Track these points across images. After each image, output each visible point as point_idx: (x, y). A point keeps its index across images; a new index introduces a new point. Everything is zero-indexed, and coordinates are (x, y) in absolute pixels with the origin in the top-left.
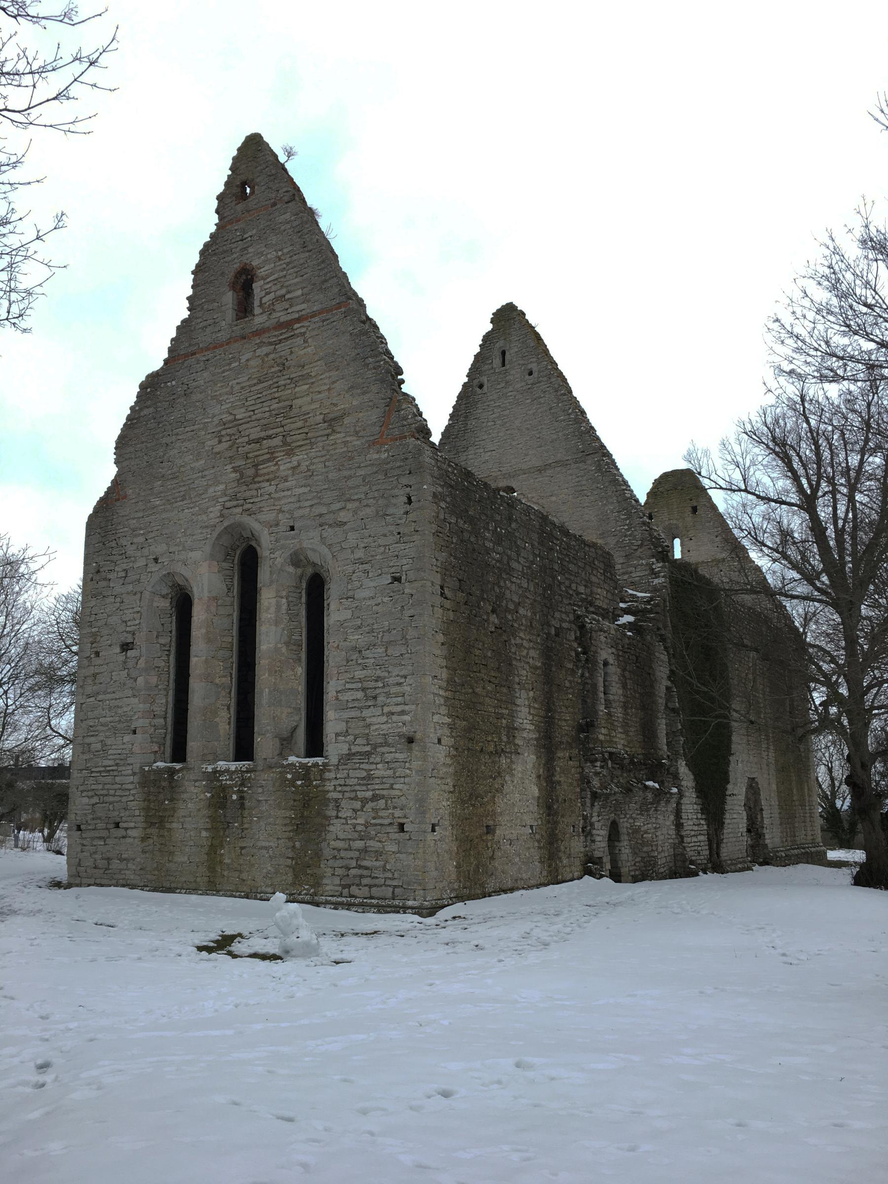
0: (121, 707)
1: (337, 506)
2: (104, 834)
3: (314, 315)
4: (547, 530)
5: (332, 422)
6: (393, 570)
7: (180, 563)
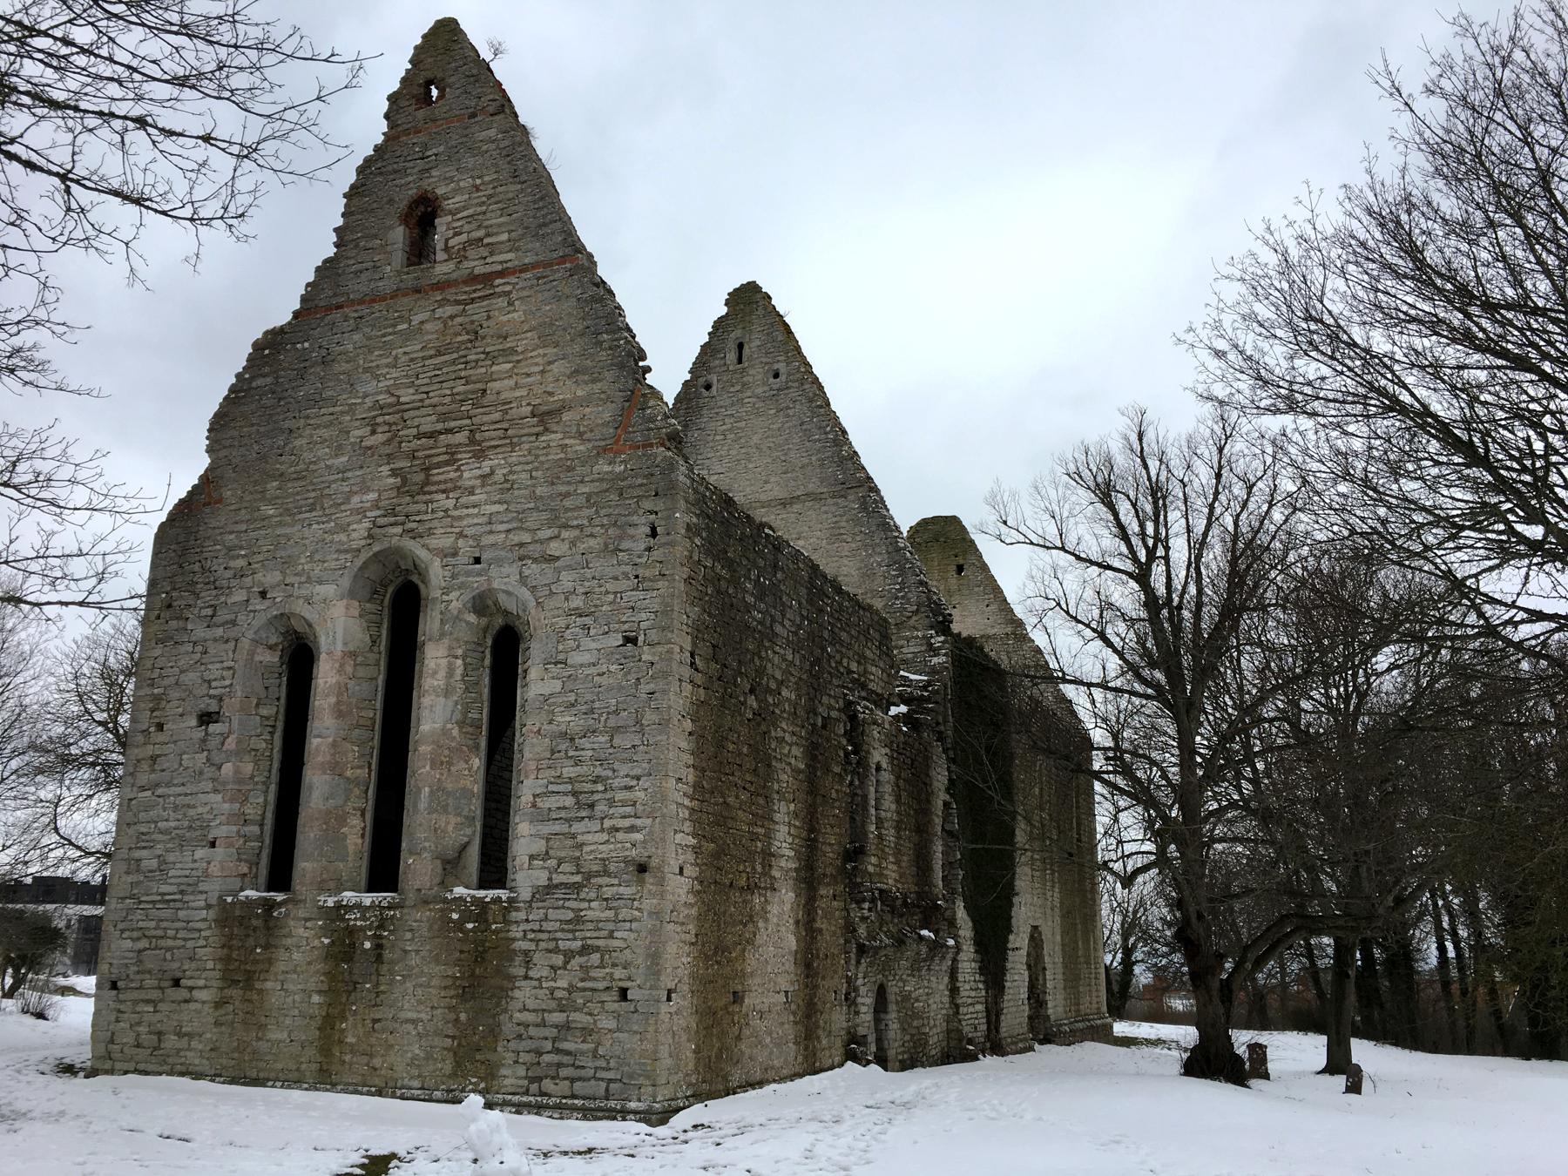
0: (194, 807)
1: (548, 533)
2: (155, 995)
3: (524, 269)
4: (819, 584)
5: (545, 417)
6: (626, 627)
7: (301, 601)
